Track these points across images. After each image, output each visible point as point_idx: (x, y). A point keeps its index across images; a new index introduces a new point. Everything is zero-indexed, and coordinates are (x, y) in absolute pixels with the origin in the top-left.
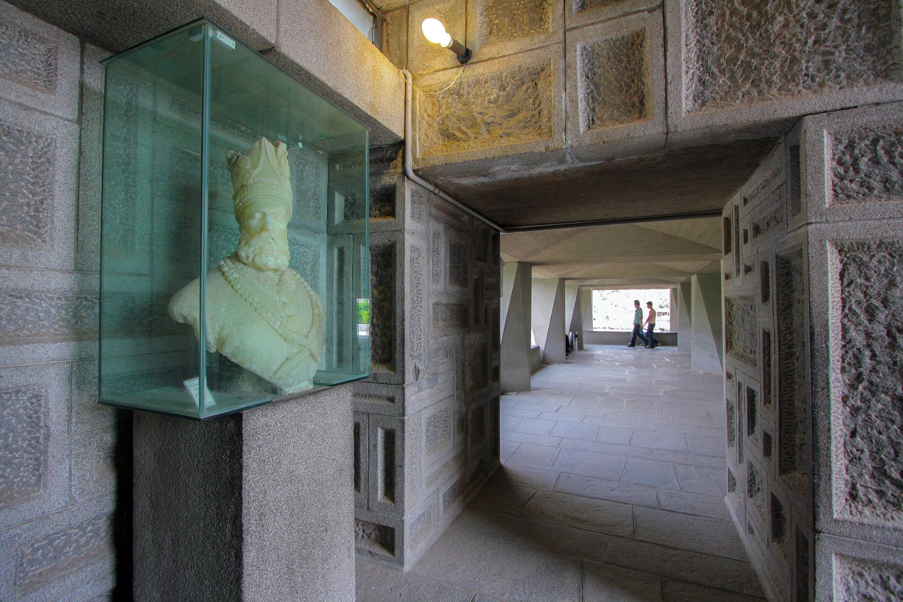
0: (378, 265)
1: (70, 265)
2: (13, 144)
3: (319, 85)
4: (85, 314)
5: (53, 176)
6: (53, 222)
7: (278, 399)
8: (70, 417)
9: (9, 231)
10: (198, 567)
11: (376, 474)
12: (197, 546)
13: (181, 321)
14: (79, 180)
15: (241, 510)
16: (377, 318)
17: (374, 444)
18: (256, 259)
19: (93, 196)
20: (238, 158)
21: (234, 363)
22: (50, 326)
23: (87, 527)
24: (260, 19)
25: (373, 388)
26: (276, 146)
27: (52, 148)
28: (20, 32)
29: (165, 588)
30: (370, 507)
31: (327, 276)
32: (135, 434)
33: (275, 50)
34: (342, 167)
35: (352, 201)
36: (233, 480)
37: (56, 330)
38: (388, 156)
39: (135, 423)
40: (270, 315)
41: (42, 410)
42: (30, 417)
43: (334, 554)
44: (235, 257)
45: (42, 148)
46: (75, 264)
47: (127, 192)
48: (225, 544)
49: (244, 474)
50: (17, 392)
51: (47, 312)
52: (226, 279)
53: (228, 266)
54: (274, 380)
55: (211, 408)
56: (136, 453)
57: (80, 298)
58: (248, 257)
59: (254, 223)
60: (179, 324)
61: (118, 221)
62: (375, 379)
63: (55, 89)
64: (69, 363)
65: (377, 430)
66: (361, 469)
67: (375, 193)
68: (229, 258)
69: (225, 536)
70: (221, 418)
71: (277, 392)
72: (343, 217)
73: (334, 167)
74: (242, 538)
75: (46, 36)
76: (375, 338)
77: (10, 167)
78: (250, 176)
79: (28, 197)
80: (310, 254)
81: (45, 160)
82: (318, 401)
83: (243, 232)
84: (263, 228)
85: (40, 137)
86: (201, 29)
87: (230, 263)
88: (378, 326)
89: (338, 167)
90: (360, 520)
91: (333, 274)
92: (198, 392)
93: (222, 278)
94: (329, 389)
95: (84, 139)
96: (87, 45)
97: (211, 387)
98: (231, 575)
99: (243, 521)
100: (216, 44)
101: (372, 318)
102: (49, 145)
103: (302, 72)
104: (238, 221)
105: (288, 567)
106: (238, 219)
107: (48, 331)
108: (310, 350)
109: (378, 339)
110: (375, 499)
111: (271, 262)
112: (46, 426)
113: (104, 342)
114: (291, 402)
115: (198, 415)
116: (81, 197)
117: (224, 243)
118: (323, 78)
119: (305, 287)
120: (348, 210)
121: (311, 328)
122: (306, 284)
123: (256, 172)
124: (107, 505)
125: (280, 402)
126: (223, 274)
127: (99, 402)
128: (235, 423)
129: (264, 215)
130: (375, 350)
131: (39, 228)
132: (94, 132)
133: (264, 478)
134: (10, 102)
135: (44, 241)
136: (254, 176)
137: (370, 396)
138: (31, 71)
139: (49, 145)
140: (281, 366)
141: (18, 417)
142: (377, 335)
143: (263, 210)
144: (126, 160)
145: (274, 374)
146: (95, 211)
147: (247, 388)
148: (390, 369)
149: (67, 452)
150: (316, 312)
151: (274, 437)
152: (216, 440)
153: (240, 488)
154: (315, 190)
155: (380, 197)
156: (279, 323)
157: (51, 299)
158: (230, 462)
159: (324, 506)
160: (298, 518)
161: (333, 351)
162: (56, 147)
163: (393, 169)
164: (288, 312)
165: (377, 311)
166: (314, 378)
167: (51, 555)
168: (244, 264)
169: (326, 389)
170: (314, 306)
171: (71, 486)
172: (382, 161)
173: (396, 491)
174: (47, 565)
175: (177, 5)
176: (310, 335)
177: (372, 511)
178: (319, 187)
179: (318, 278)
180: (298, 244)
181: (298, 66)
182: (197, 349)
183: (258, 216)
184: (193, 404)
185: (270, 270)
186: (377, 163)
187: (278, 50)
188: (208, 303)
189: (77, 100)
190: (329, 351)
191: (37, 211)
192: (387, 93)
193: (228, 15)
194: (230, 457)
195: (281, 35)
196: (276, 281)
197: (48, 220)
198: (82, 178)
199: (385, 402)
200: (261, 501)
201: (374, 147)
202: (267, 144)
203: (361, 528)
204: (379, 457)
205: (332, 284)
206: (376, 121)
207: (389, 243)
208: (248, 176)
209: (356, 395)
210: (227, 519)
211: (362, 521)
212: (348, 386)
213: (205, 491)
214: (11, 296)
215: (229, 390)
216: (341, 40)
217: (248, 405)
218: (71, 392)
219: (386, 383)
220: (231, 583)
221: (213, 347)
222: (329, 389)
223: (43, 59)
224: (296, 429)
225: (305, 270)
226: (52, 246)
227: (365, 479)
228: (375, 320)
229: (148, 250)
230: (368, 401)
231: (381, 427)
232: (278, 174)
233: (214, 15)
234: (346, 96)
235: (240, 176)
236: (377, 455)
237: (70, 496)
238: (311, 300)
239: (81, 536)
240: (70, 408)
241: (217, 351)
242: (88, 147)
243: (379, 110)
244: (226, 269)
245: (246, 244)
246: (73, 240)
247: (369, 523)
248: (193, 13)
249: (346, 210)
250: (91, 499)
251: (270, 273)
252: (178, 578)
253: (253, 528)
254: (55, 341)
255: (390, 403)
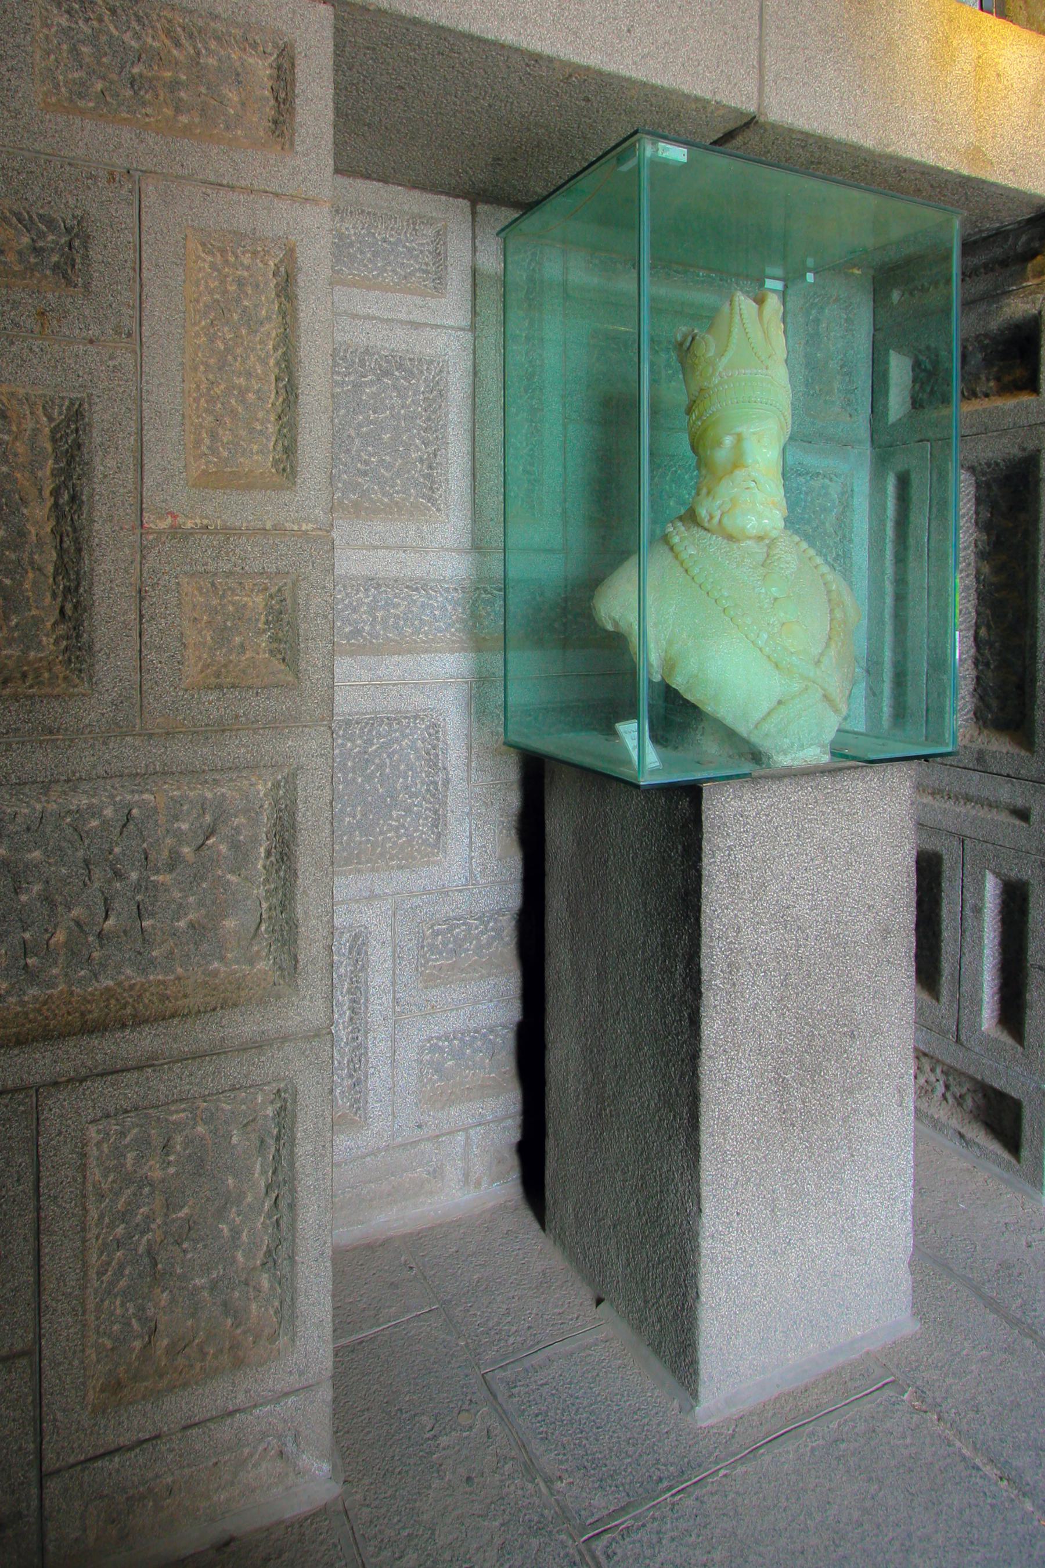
0: (994, 507)
1: (466, 541)
2: (405, 378)
3: (846, 153)
4: (483, 613)
5: (446, 416)
6: (447, 480)
7: (762, 773)
8: (469, 759)
9: (403, 500)
10: (633, 1021)
11: (978, 973)
12: (632, 988)
13: (610, 627)
14: (474, 414)
15: (699, 946)
16: (989, 627)
17: (976, 905)
18: (725, 521)
19: (493, 434)
20: (693, 339)
21: (688, 701)
22: (446, 629)
23: (489, 922)
24: (728, 77)
25: (975, 783)
26: (760, 301)
27: (444, 375)
28: (408, 221)
29: (587, 1040)
30: (963, 1038)
31: (870, 534)
32: (547, 798)
33: (757, 122)
34: (907, 295)
35: (929, 367)
36: (687, 894)
37: (453, 635)
38: (1019, 249)
39: (547, 781)
40: (749, 620)
41: (441, 746)
42: (428, 753)
43: (868, 1088)
44: (691, 518)
45: (434, 377)
46: (473, 539)
47: (532, 421)
48: (674, 997)
49: (705, 889)
50: (416, 717)
51: (443, 608)
52: (676, 557)
53: (679, 534)
54: (755, 739)
55: (653, 771)
56: (549, 828)
57: (478, 588)
58: (711, 518)
59: (722, 455)
60: (606, 631)
61: (521, 468)
62: (981, 762)
63: (445, 288)
64: (467, 682)
65: (984, 876)
66: (943, 951)
67: (986, 342)
68: (681, 518)
69: (675, 983)
70: (669, 790)
71: (760, 759)
72: (909, 404)
73: (888, 296)
74: (701, 993)
75: (434, 214)
76: (982, 671)
77: (402, 412)
78: (714, 370)
79: (421, 450)
80: (834, 490)
81: (437, 393)
82: (838, 787)
83: (704, 472)
84: (737, 462)
85: (432, 362)
86: (634, 151)
87: (683, 529)
88: (991, 645)
89: (896, 296)
90: (938, 1061)
91: (885, 530)
92: (636, 742)
93: (671, 555)
94: (862, 767)
95: (479, 352)
96: (481, 208)
97: (655, 739)
98: (682, 1047)
99: (702, 965)
100: (661, 166)
101: (977, 627)
102: (441, 371)
103: (811, 141)
104: (694, 452)
105: (777, 1073)
106: (694, 449)
107: (444, 636)
108: (823, 689)
109: (990, 674)
110: (975, 1026)
111: (751, 524)
112: (445, 769)
113: (510, 655)
114: (786, 781)
115: (637, 779)
116: (477, 439)
117: (670, 487)
118: (855, 137)
119: (816, 567)
120: (921, 387)
121: (827, 645)
122: (819, 560)
123: (725, 360)
124: (511, 898)
125: (766, 777)
126: (672, 549)
127: (505, 743)
128: (690, 802)
129: (739, 439)
130: (981, 698)
131: (433, 492)
132: (491, 334)
133: (737, 904)
134: (401, 322)
135: (439, 510)
136: (720, 369)
137: (968, 799)
138: (420, 270)
139: (441, 371)
140: (769, 714)
141: (417, 750)
142: (987, 665)
143: (738, 430)
144: (530, 370)
145: (756, 727)
146: (493, 458)
147: (710, 747)
148: (1020, 744)
149: (466, 810)
150: (838, 614)
151: (754, 838)
152: (661, 825)
153: (698, 910)
154: (845, 355)
155: (1000, 348)
156: (765, 636)
157: (447, 590)
158: (682, 863)
159: (848, 990)
160: (797, 994)
161: (882, 692)
162: (448, 372)
163: (1034, 277)
164: (782, 615)
165: (988, 612)
166: (832, 742)
167: (451, 946)
168: (706, 529)
169: (856, 768)
170: (833, 604)
171: (472, 858)
172: (1004, 263)
173: (1028, 1021)
174: (447, 959)
175: (598, 112)
176: (825, 660)
177: (968, 1049)
178: (853, 348)
179: (851, 541)
180: (807, 473)
181: (802, 133)
182: (634, 673)
183: (728, 441)
184: (628, 762)
185: (750, 538)
186: (992, 270)
187: (762, 119)
188: (650, 599)
189: (469, 296)
190: (873, 693)
191: (430, 467)
192: (1015, 107)
193: (674, 97)
194: (683, 857)
195: (767, 89)
196: (761, 558)
197: (442, 478)
198: (477, 412)
199: (1004, 818)
200: (731, 942)
201: (984, 235)
202: (744, 303)
203: (942, 1078)
204: (986, 935)
205: (882, 551)
206: (984, 182)
207: (1020, 454)
208: (711, 370)
209: (920, 788)
210: (677, 956)
211: (944, 1064)
212: (904, 766)
213: (645, 904)
214: (407, 587)
215: (680, 748)
216: (895, 36)
217: (712, 775)
218: (470, 725)
219: (1008, 776)
220: (683, 1061)
221: (657, 672)
222: (862, 767)
223: (431, 248)
224: (794, 831)
225: (823, 523)
226: (447, 515)
227: (952, 975)
228: (983, 632)
229: (559, 510)
230: (961, 809)
231: (994, 872)
232: (763, 358)
233: (651, 105)
234: (908, 155)
235: (698, 373)
236: (981, 930)
237: (471, 872)
238: (829, 592)
239: (482, 933)
240: (470, 748)
241: (663, 679)
242: (484, 363)
243: (990, 155)
244: (676, 540)
245: (708, 493)
246: (468, 505)
247: (962, 1074)
248: (620, 114)
249: (917, 387)
250: (493, 882)
251: (749, 542)
252: (605, 1031)
253: (718, 982)
254: (452, 651)
255: (1017, 822)
